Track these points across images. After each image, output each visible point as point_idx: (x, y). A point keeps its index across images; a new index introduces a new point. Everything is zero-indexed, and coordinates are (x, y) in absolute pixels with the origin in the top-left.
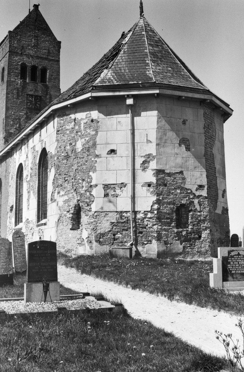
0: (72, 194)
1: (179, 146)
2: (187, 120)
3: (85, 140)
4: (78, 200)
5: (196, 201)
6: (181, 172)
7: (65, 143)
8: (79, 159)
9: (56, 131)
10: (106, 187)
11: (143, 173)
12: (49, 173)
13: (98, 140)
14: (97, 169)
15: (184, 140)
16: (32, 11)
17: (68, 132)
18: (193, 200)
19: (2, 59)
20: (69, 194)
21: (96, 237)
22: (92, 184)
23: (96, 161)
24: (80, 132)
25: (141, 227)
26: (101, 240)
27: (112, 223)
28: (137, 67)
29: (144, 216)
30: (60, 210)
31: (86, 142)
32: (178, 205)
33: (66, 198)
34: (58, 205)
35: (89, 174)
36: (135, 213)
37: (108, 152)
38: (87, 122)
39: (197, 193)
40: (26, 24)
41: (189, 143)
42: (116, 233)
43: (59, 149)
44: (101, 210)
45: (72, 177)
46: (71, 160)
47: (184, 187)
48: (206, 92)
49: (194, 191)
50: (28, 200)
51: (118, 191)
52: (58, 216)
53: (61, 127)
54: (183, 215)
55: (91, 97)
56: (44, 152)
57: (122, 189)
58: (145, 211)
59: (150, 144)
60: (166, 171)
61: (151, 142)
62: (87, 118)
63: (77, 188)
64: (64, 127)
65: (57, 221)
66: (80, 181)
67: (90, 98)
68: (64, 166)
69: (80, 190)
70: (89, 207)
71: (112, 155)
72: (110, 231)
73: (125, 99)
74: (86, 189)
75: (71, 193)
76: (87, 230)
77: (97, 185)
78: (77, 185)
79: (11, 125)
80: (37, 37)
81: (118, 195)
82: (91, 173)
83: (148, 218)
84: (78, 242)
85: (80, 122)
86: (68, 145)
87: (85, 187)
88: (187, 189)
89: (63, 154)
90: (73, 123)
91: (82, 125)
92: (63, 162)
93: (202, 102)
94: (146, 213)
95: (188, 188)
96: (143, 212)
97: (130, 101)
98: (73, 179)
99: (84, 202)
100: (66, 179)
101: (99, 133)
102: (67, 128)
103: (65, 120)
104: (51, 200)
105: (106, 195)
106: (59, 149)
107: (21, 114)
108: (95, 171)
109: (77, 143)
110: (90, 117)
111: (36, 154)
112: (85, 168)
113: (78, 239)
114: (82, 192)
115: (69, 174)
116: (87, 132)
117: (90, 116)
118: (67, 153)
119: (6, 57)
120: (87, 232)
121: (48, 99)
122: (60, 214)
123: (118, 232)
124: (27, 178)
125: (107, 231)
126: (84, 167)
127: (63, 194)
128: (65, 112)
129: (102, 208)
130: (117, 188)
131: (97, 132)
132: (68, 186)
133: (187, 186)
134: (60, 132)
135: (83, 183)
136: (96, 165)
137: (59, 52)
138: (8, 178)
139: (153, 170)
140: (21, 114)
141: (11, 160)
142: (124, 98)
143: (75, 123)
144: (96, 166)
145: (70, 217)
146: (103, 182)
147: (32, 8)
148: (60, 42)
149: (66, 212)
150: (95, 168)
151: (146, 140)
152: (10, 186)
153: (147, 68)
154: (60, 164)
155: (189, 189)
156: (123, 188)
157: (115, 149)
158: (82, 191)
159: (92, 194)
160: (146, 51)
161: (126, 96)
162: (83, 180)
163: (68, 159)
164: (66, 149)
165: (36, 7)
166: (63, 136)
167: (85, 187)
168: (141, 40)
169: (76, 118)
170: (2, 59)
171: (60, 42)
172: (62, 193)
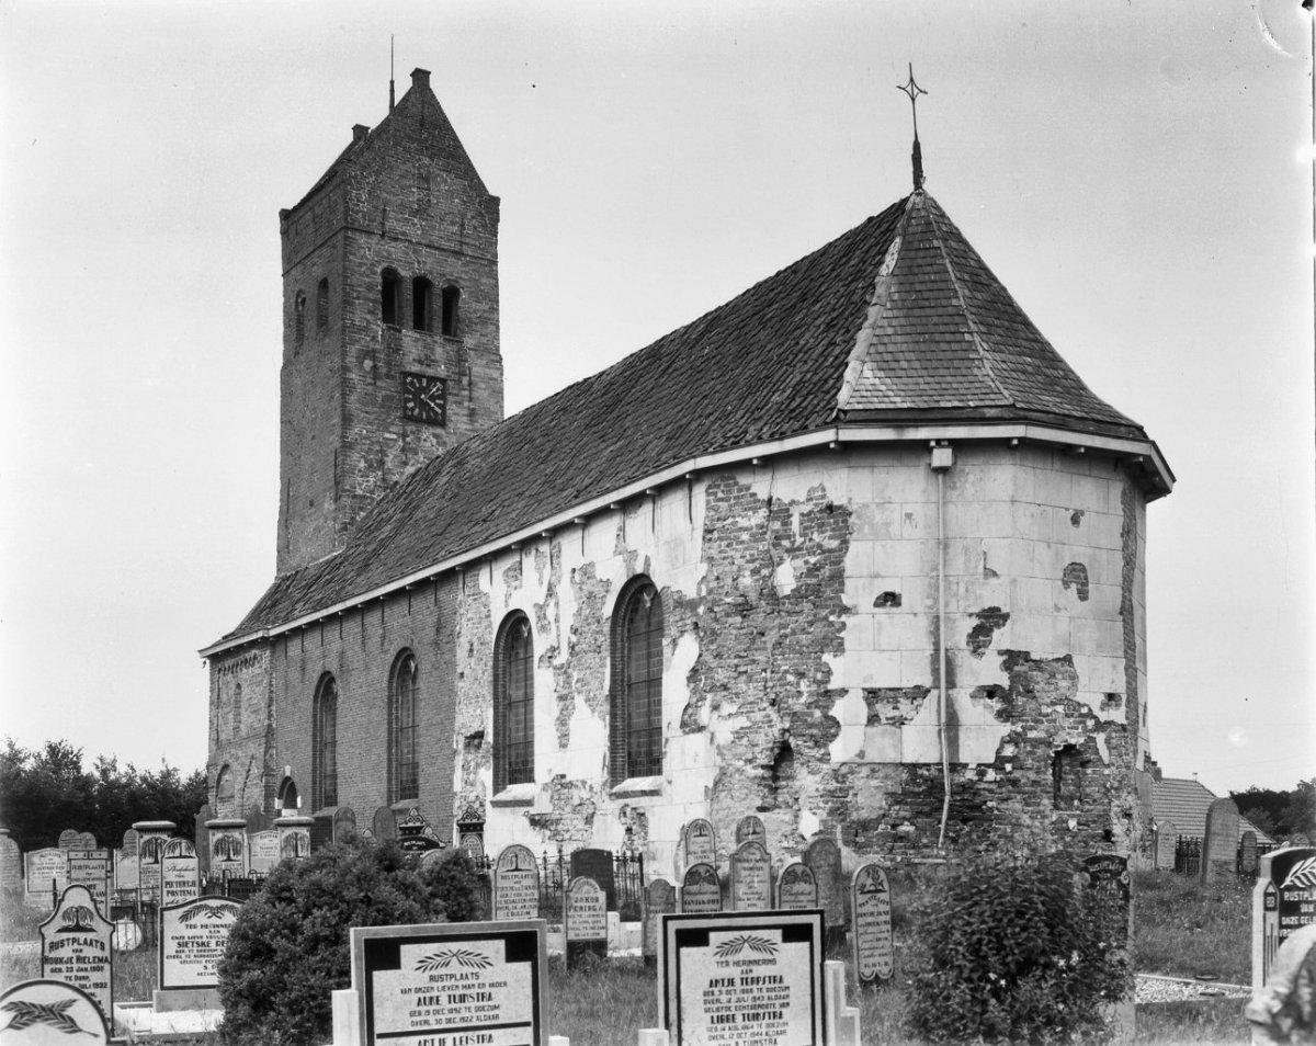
0: (763, 713)
1: (1062, 587)
2: (1083, 513)
3: (806, 562)
4: (785, 731)
5: (1100, 738)
6: (1068, 659)
7: (735, 568)
8: (783, 614)
9: (699, 533)
10: (872, 695)
11: (974, 661)
12: (667, 651)
13: (849, 563)
14: (846, 645)
15: (1074, 570)
16: (405, 99)
17: (745, 536)
18: (1095, 735)
19: (314, 250)
20: (753, 712)
21: (845, 831)
22: (830, 687)
23: (844, 624)
24: (788, 537)
25: (968, 807)
26: (861, 839)
27: (892, 794)
28: (941, 354)
29: (976, 778)
30: (720, 754)
31: (809, 570)
32: (1060, 749)
33: (742, 722)
34: (716, 742)
35: (820, 658)
36: (956, 767)
37: (877, 598)
38: (810, 512)
39: (1103, 717)
40: (394, 136)
41: (1086, 578)
42: (898, 822)
43: (713, 584)
44: (858, 760)
45: (762, 666)
46: (758, 618)
47: (1075, 699)
48: (1133, 433)
49: (1097, 712)
50: (562, 722)
51: (905, 707)
52: (713, 774)
53: (718, 519)
54: (1064, 776)
55: (836, 442)
56: (638, 589)
57: (916, 703)
58: (979, 765)
59: (993, 581)
60: (1034, 656)
61: (995, 574)
62: (811, 499)
63: (781, 695)
64: (730, 520)
65: (711, 785)
66: (791, 678)
67: (832, 446)
68: (734, 632)
69: (790, 701)
70: (822, 751)
71: (888, 609)
72: (884, 816)
73: (930, 451)
74: (810, 700)
75: (760, 710)
76: (814, 813)
77: (847, 691)
78: (778, 689)
79: (360, 471)
80: (427, 180)
81: (906, 719)
82: (827, 657)
83: (986, 782)
84: (785, 844)
85: (788, 510)
86: (747, 573)
87: (806, 695)
88: (1079, 704)
89: (729, 600)
90: (763, 512)
91: (795, 520)
92: (730, 620)
93: (1118, 461)
94: (981, 770)
95: (1082, 702)
96: (974, 766)
97: (942, 457)
98: (765, 670)
99: (804, 735)
100: (742, 669)
101: (853, 546)
102: (739, 525)
103: (732, 501)
104: (683, 725)
105: (873, 719)
106: (713, 584)
107: (387, 435)
108: (839, 649)
109: (780, 570)
110: (824, 497)
111: (598, 590)
112: (804, 642)
113: (786, 836)
114: (797, 708)
115: (751, 658)
116: (811, 539)
117: (820, 493)
118: (742, 596)
119: (334, 247)
120: (814, 817)
121: (464, 390)
122: (721, 768)
123: (904, 818)
124: (550, 657)
125: (874, 816)
126: (804, 638)
127: (733, 711)
128: (734, 478)
129: (861, 754)
130: (901, 700)
131: (845, 542)
132: (752, 691)
133: (1080, 697)
134: (716, 535)
135: (798, 684)
136: (842, 635)
137: (495, 234)
138: (452, 651)
139: (1001, 653)
140: (387, 435)
141: (460, 597)
142: (923, 447)
143: (770, 511)
144: (842, 639)
145: (756, 777)
146: (865, 681)
147: (404, 85)
148: (496, 201)
149: (742, 763)
150: (841, 644)
151: (981, 569)
152: (462, 674)
153: (971, 356)
154: (717, 627)
155: (1085, 705)
156: (919, 700)
157: (897, 591)
158: (798, 705)
159: (830, 713)
160: (954, 302)
161: (933, 444)
162: (801, 675)
163: (748, 613)
164: (741, 587)
165: (421, 76)
166: (728, 546)
167: (806, 695)
168: (935, 267)
169: (774, 499)
170: (314, 250)
171: (496, 201)
172: (727, 708)
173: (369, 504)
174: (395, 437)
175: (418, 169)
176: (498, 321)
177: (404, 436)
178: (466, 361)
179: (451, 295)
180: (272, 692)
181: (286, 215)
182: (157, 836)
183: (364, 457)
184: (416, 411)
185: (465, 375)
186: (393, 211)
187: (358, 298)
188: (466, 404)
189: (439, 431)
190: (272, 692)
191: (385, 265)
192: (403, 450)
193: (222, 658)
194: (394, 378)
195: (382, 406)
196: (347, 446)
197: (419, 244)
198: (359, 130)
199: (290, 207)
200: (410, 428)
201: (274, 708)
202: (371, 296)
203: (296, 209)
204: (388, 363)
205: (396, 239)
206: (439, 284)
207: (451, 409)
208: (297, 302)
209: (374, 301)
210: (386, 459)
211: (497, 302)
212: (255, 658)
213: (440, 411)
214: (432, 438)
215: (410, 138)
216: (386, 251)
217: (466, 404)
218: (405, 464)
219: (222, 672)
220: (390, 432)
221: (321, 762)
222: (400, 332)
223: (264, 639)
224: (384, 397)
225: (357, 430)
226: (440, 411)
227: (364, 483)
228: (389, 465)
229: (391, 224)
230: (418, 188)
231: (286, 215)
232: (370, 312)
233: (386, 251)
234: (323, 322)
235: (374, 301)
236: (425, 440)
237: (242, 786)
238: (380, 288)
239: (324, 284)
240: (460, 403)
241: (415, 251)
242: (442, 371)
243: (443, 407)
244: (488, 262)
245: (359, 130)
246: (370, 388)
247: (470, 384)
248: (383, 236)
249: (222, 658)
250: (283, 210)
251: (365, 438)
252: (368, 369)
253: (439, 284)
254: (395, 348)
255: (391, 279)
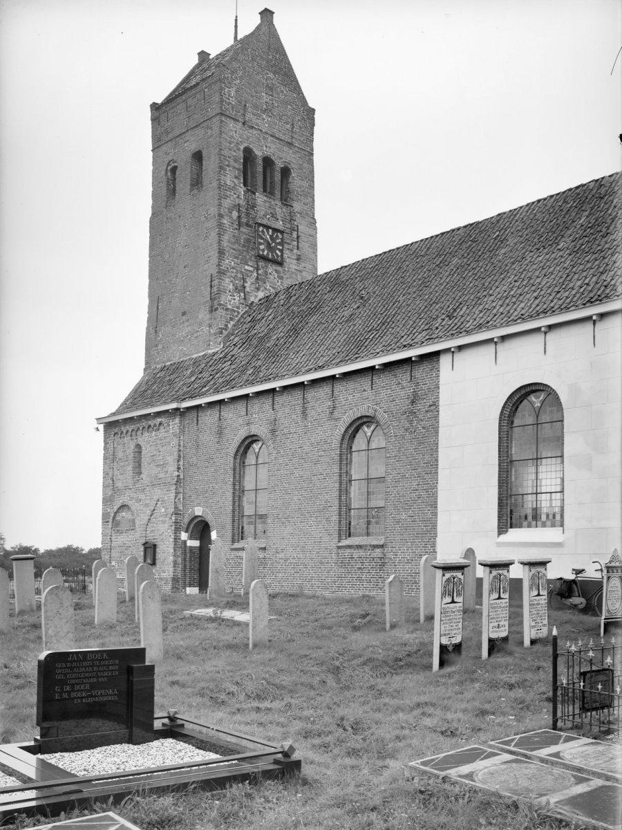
19: (188, 131)
80: (271, 89)
107: (247, 267)
147: (250, 24)
148: (313, 110)
165: (267, 14)
173: (237, 316)
174: (252, 269)
175: (266, 80)
176: (314, 195)
177: (258, 269)
178: (295, 220)
179: (286, 172)
180: (180, 451)
181: (155, 107)
182: (455, 574)
183: (231, 281)
184: (265, 253)
185: (295, 231)
186: (251, 107)
187: (228, 166)
188: (295, 251)
189: (279, 268)
190: (180, 451)
191: (246, 145)
192: (257, 278)
193: (112, 426)
194: (251, 226)
195: (244, 246)
196: (221, 273)
197: (267, 133)
198: (203, 55)
199: (159, 101)
200: (261, 264)
201: (181, 463)
202: (236, 165)
203: (163, 104)
204: (248, 214)
205: (252, 127)
206: (279, 165)
207: (287, 254)
208: (167, 170)
209: (239, 169)
210: (246, 285)
211: (313, 182)
212: (160, 424)
213: (279, 254)
214: (274, 273)
215: (262, 57)
216: (234, 142)
217: (295, 251)
218: (258, 289)
219: (140, 432)
220: (248, 265)
221: (239, 505)
222: (254, 194)
223: (177, 409)
224: (245, 239)
225: (228, 262)
226: (279, 254)
227: (232, 300)
228: (247, 289)
229: (249, 116)
230: (266, 93)
231: (155, 107)
232: (236, 177)
233: (234, 142)
234: (197, 183)
235: (239, 169)
236: (270, 274)
237: (145, 522)
238: (242, 161)
239: (198, 157)
240: (292, 250)
241: (264, 138)
242: (279, 225)
243: (281, 251)
244: (308, 154)
245: (203, 55)
246: (236, 231)
247: (298, 237)
248: (244, 124)
249: (112, 426)
250: (154, 103)
251: (233, 268)
252: (235, 218)
253: (279, 165)
254: (252, 206)
255: (248, 154)
